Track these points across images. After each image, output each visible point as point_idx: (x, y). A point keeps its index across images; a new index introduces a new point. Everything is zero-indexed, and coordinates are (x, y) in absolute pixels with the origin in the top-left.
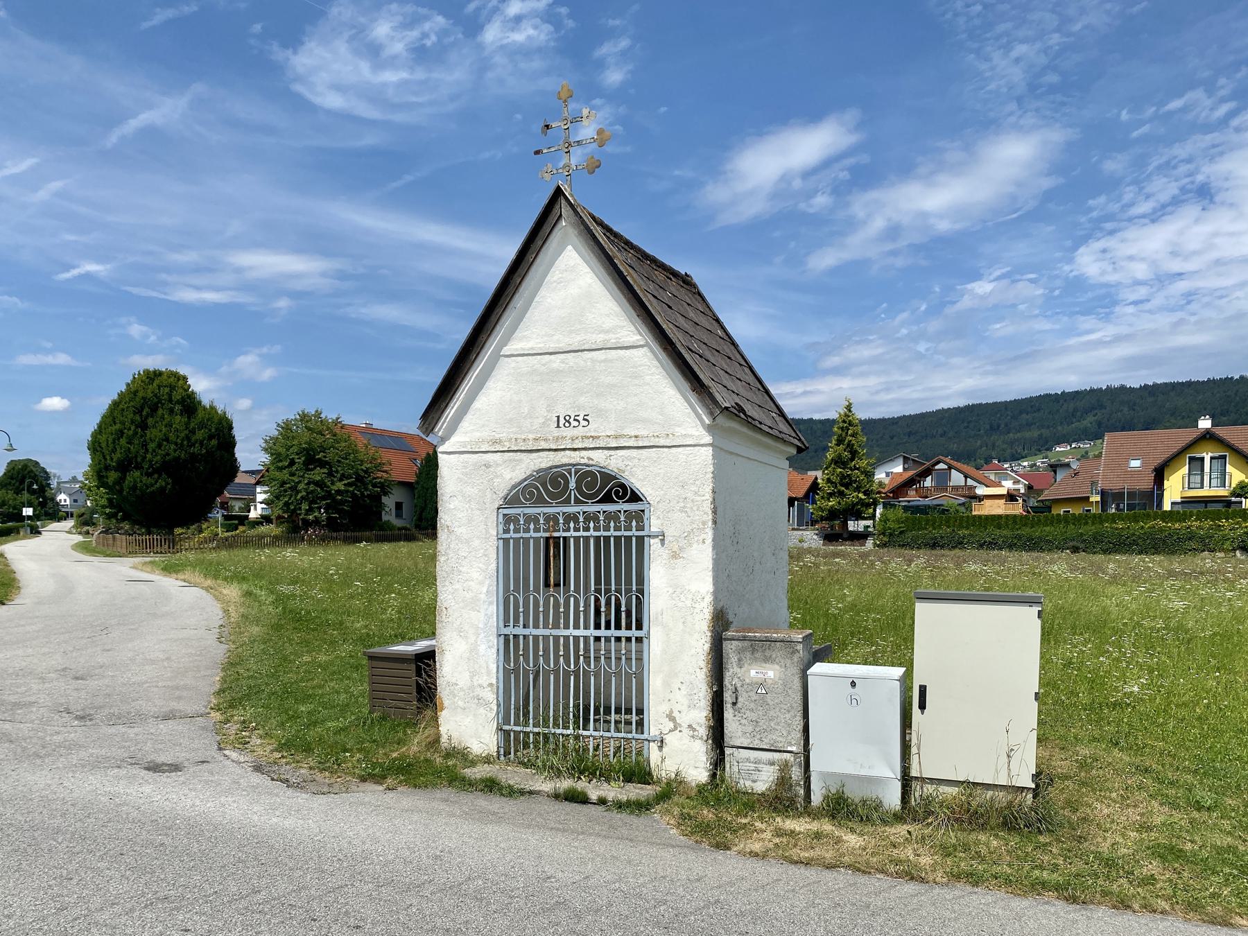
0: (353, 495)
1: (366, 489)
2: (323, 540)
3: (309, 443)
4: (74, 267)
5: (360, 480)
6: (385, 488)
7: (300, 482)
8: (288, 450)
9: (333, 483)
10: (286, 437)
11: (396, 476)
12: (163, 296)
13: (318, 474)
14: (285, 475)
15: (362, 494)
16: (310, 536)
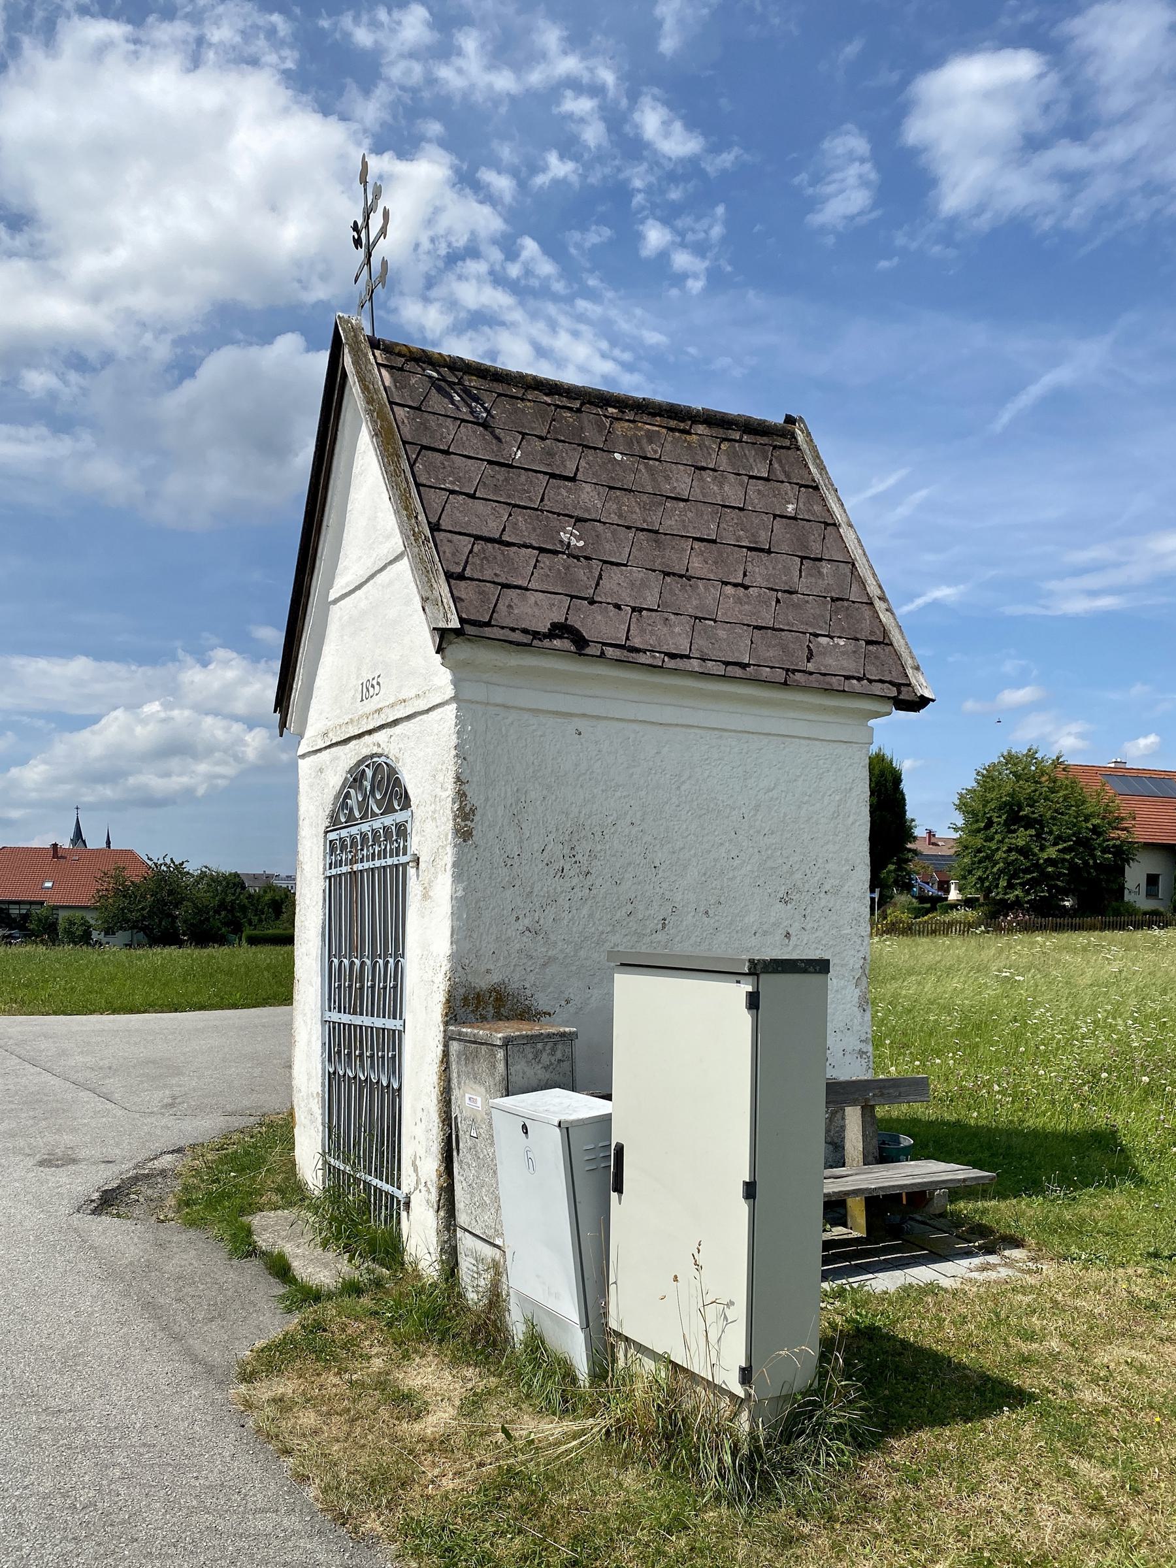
0: (1073, 866)
1: (1094, 857)
2: (1027, 928)
3: (1012, 795)
4: (919, 596)
5: (1083, 844)
6: (1123, 854)
7: (998, 849)
8: (985, 806)
9: (1042, 849)
10: (988, 790)
11: (1141, 835)
12: (1044, 612)
13: (1022, 837)
14: (979, 841)
15: (1086, 863)
16: (1010, 923)
